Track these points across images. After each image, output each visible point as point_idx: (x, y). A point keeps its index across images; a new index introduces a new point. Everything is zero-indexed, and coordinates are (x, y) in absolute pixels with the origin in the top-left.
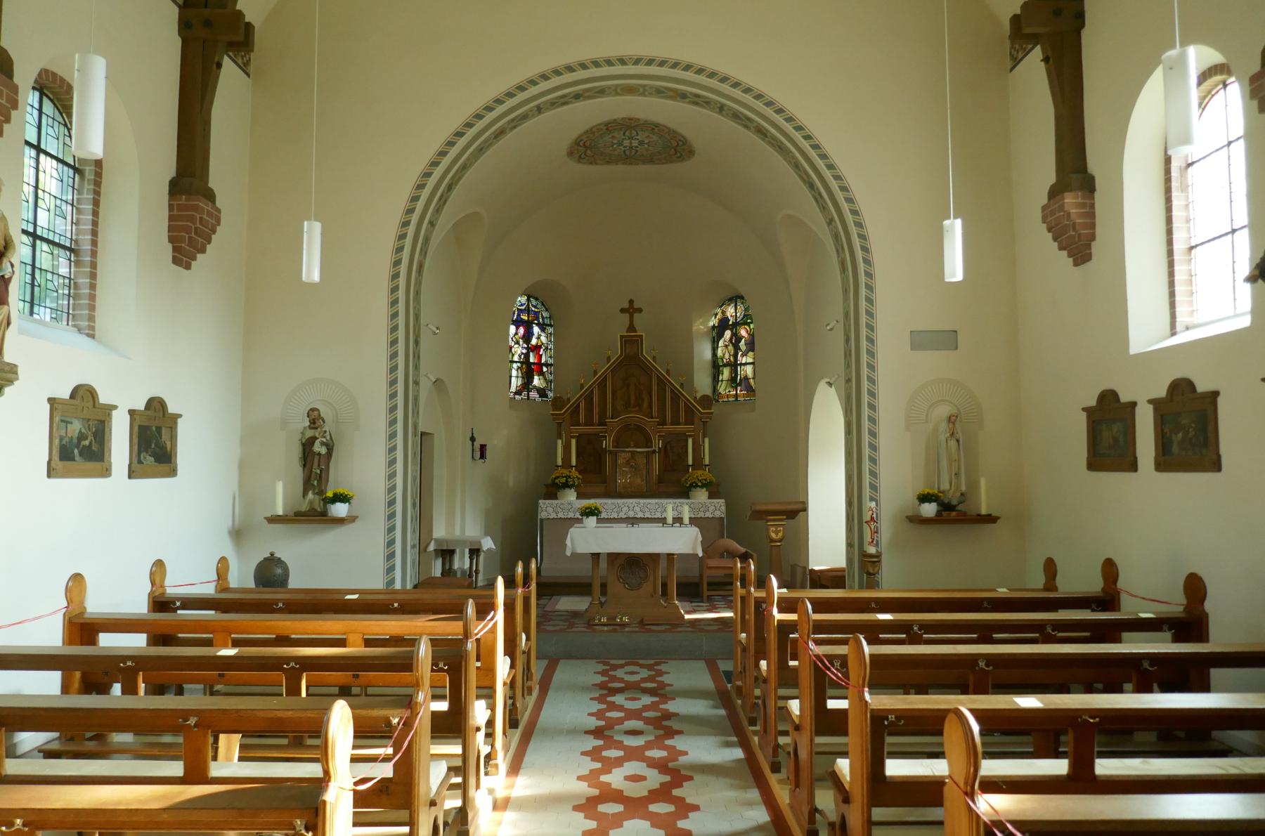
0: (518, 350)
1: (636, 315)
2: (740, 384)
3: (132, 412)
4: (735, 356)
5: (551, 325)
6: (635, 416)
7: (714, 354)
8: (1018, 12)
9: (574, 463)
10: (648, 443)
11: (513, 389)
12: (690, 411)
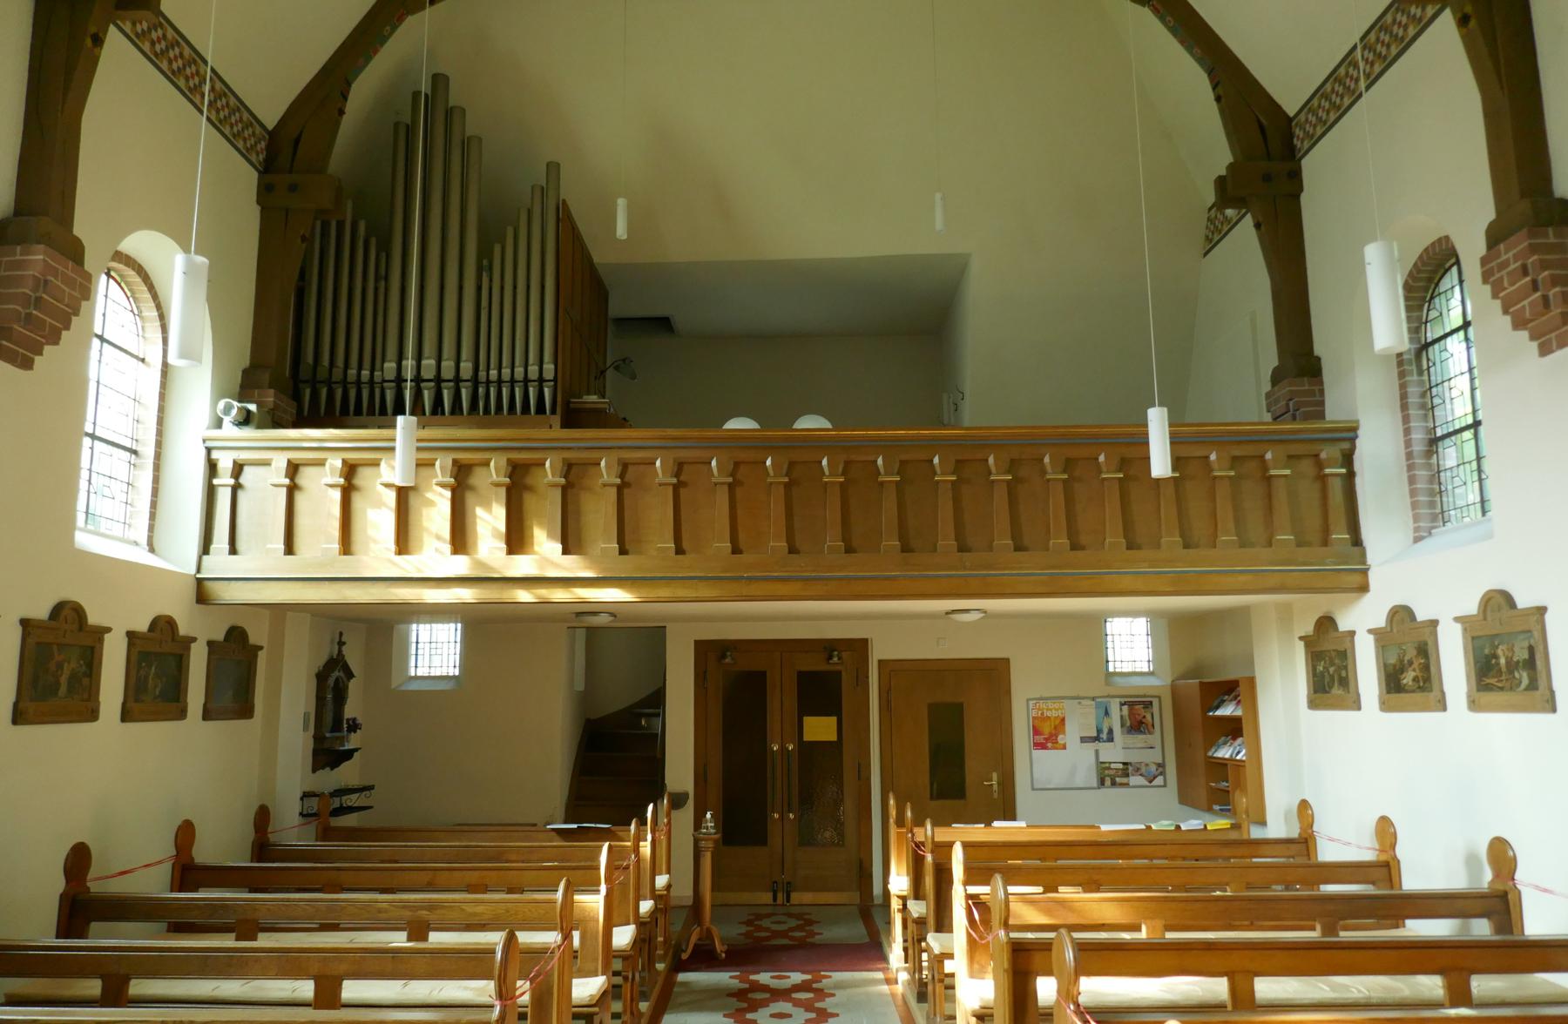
3: (131, 635)
8: (1223, 172)
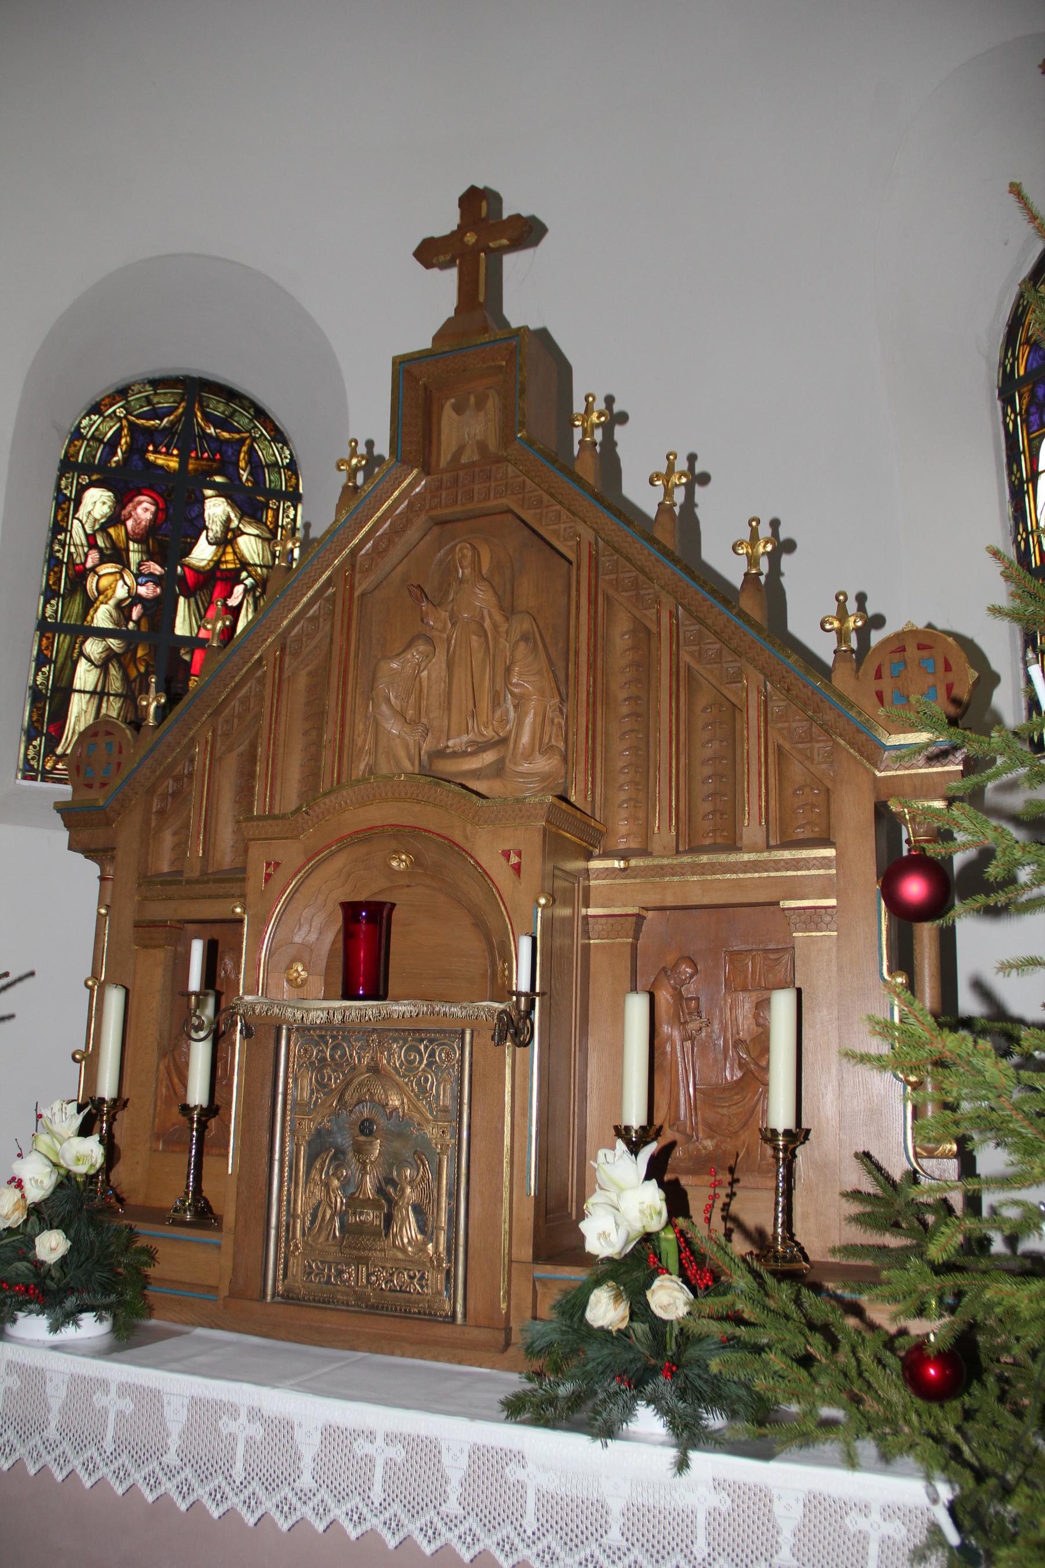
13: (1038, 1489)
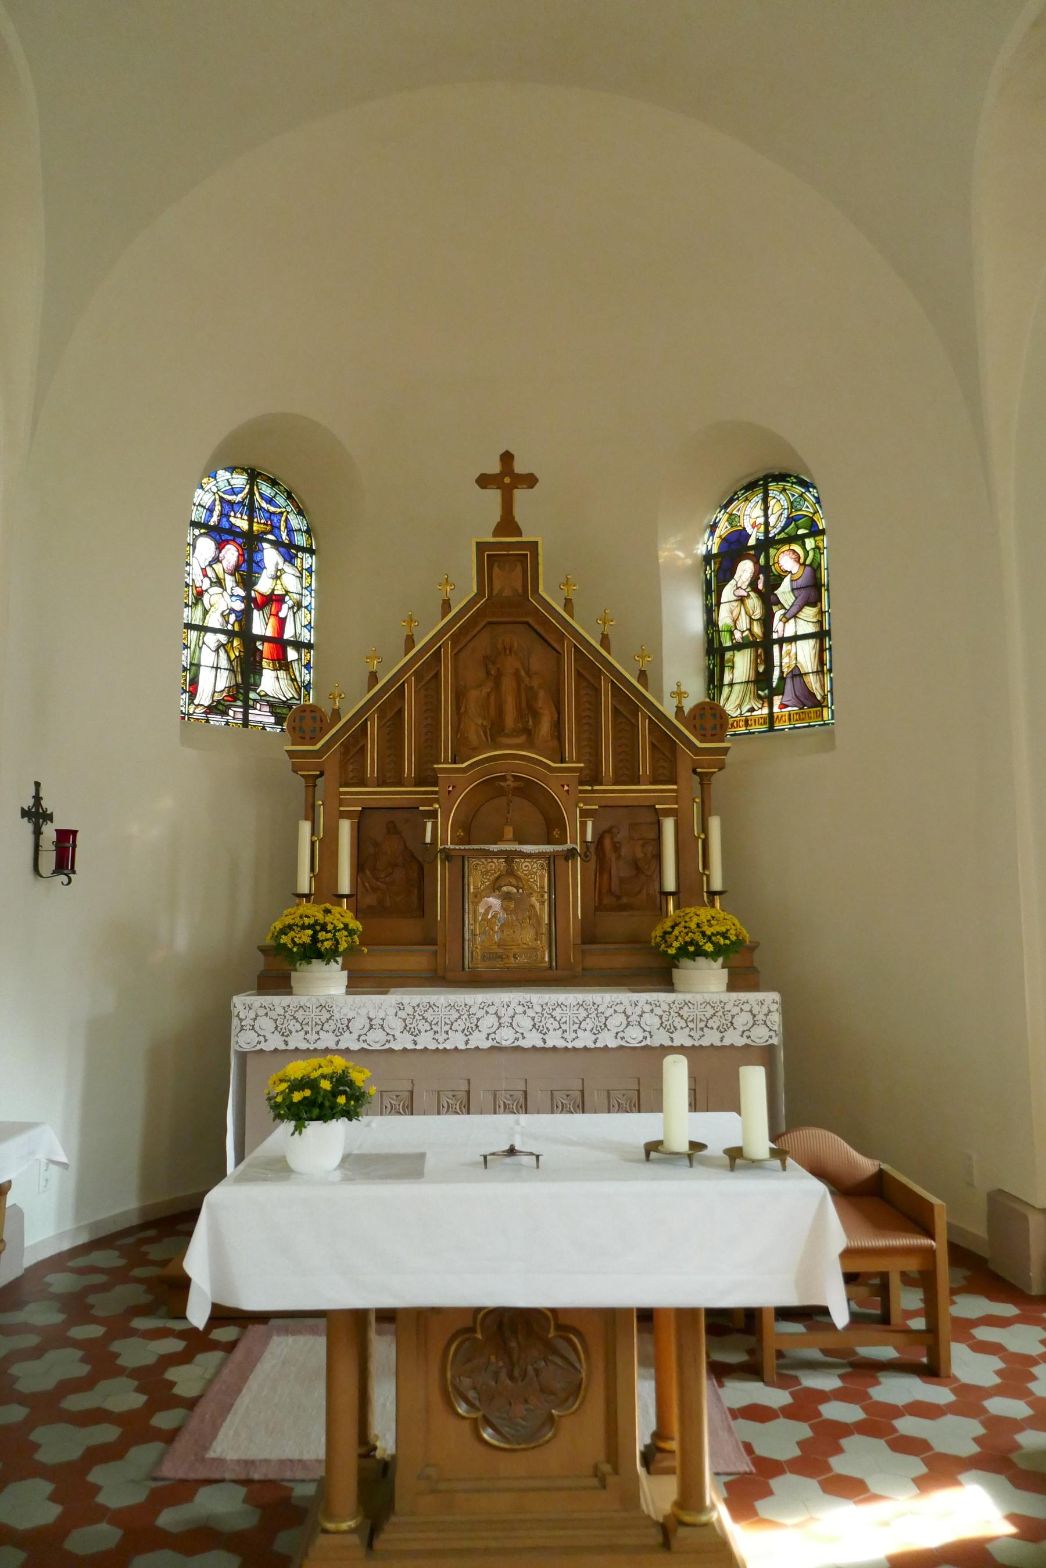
0: (222, 603)
1: (520, 495)
2: (780, 691)
4: (767, 621)
5: (311, 551)
6: (515, 756)
7: (711, 622)
9: (345, 886)
10: (552, 827)
11: (204, 696)
12: (666, 744)
13: (522, 1380)
